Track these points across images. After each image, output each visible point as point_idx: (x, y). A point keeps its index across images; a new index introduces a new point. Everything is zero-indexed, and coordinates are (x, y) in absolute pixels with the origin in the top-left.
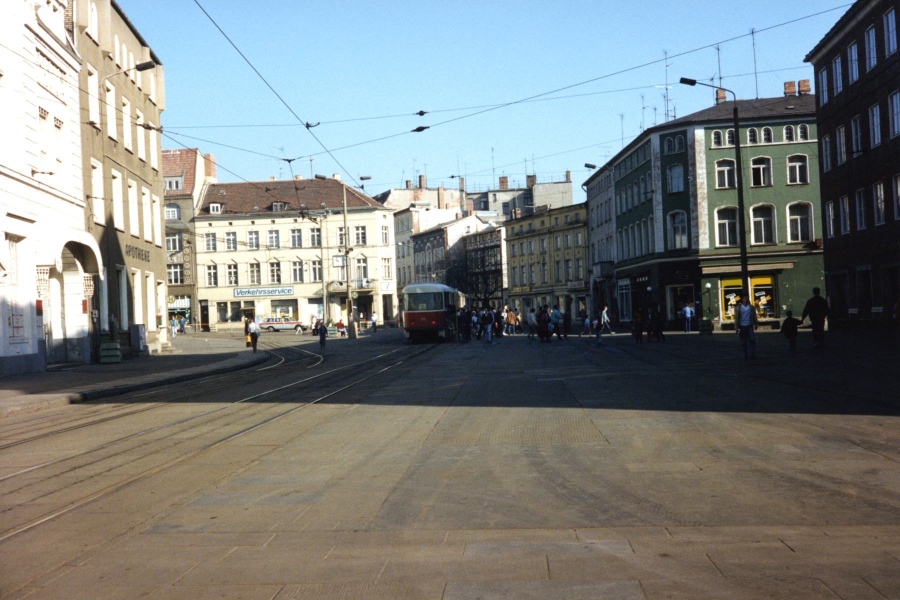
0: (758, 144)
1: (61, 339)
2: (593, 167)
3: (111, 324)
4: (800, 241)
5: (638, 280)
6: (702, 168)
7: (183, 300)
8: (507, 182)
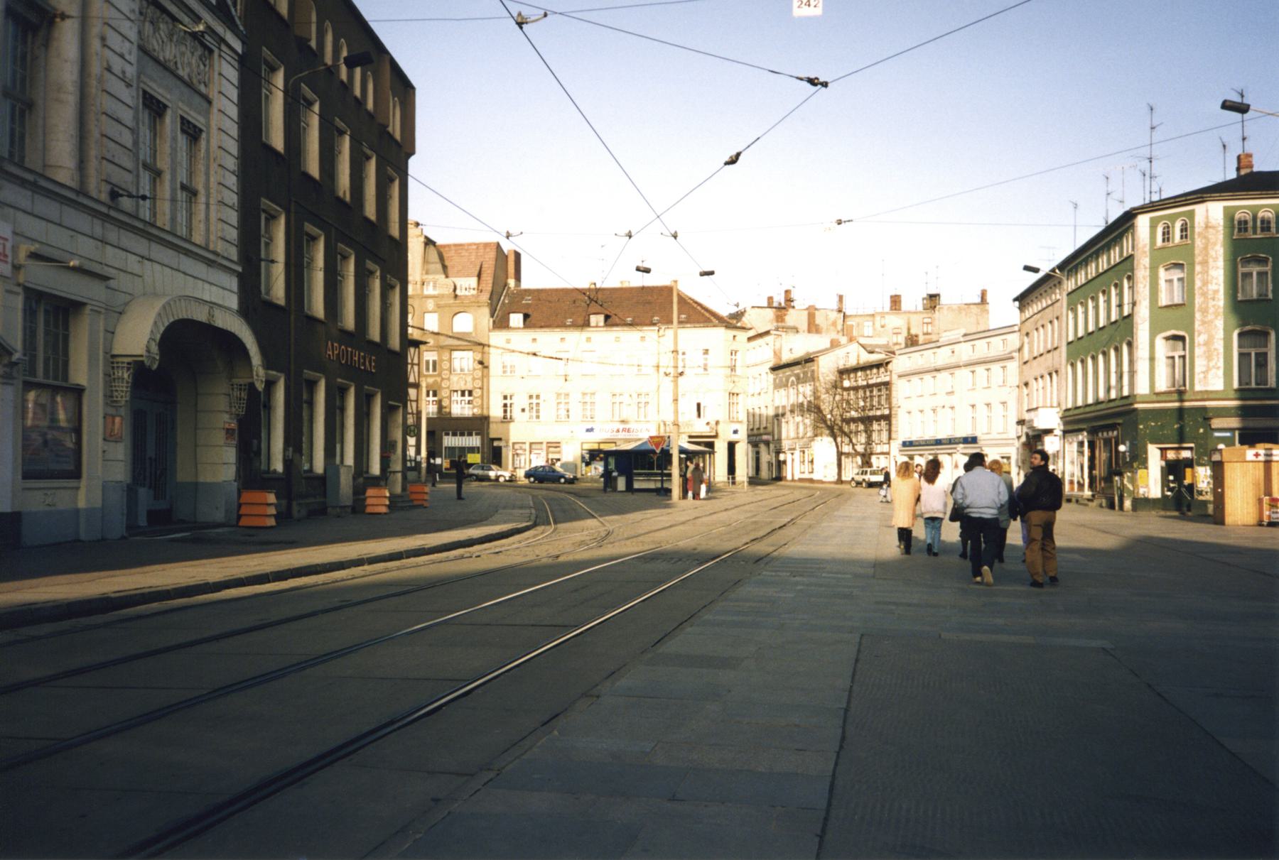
0: (1240, 266)
2: (1036, 270)
3: (287, 463)
6: (1218, 268)
7: (471, 438)
8: (900, 302)
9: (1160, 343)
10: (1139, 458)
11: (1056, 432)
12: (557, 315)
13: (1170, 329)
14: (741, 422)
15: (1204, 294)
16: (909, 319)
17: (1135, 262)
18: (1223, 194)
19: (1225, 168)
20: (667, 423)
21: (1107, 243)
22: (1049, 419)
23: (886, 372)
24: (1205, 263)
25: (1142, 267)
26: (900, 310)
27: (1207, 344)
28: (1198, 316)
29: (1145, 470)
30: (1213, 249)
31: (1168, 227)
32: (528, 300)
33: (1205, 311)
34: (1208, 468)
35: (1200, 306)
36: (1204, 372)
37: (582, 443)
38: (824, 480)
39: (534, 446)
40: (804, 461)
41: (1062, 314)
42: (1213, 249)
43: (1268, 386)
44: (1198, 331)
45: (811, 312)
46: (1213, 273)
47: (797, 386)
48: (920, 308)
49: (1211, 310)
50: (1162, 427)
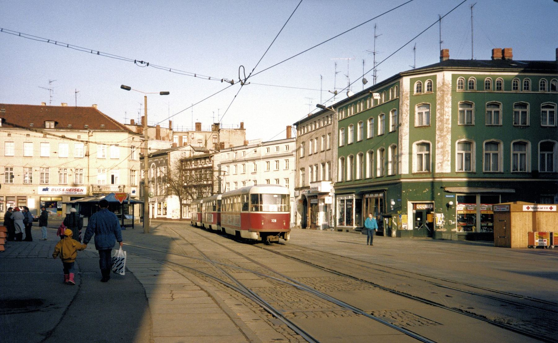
1: (427, 148)
4: (464, 171)
5: (427, 189)
10: (401, 208)
11: (330, 194)
13: (420, 140)
14: (136, 186)
15: (442, 121)
16: (206, 135)
20: (94, 186)
21: (381, 90)
24: (442, 104)
27: (442, 147)
29: (406, 215)
30: (446, 97)
31: (421, 84)
33: (441, 130)
36: (441, 163)
38: (173, 218)
41: (334, 131)
42: (446, 97)
44: (438, 141)
45: (158, 129)
49: (445, 130)
50: (416, 192)
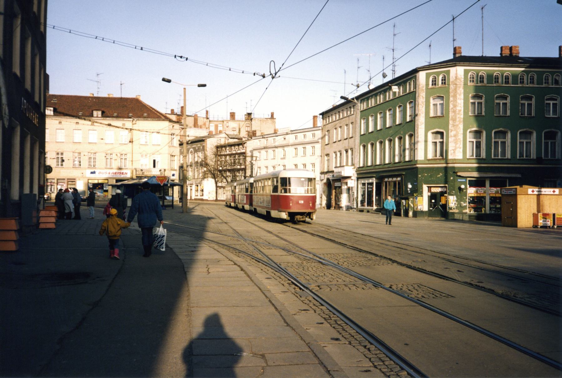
6: (461, 99)
9: (430, 135)
10: (416, 191)
11: (352, 178)
12: (73, 110)
14: (176, 170)
17: (417, 95)
18: (465, 63)
19: (430, 56)
20: (137, 170)
22: (349, 171)
23: (243, 148)
24: (455, 96)
25: (421, 97)
26: (235, 119)
27: (455, 136)
28: (451, 122)
29: (422, 197)
31: (435, 78)
32: (55, 101)
33: (454, 120)
34: (455, 196)
35: (452, 117)
36: (453, 150)
37: (88, 180)
38: (209, 199)
39: (59, 181)
40: (198, 190)
41: (356, 121)
43: (481, 158)
46: (459, 101)
47: (194, 153)
48: (244, 120)
49: (458, 120)
50: (431, 176)
